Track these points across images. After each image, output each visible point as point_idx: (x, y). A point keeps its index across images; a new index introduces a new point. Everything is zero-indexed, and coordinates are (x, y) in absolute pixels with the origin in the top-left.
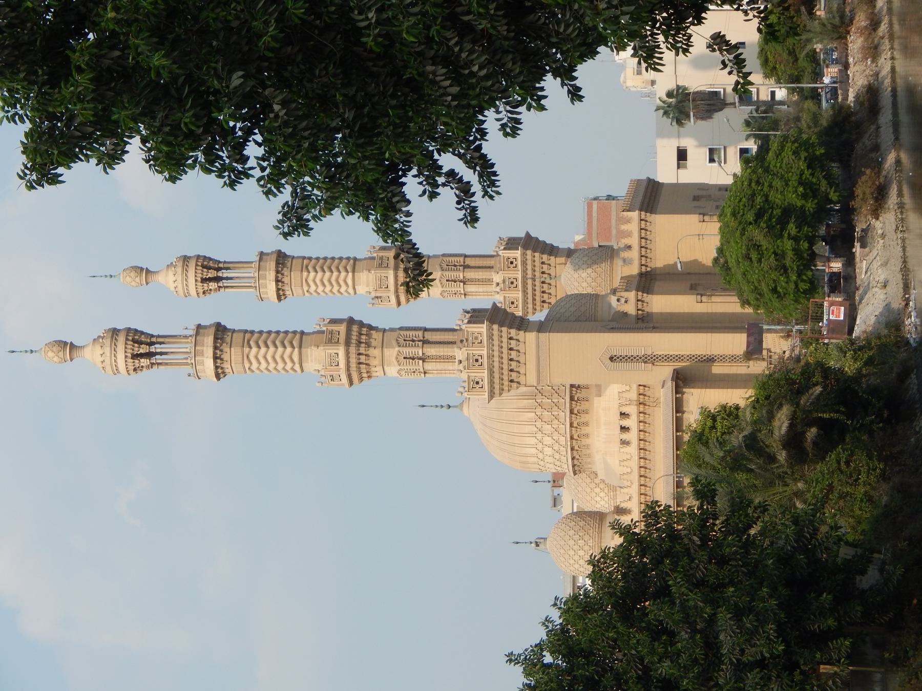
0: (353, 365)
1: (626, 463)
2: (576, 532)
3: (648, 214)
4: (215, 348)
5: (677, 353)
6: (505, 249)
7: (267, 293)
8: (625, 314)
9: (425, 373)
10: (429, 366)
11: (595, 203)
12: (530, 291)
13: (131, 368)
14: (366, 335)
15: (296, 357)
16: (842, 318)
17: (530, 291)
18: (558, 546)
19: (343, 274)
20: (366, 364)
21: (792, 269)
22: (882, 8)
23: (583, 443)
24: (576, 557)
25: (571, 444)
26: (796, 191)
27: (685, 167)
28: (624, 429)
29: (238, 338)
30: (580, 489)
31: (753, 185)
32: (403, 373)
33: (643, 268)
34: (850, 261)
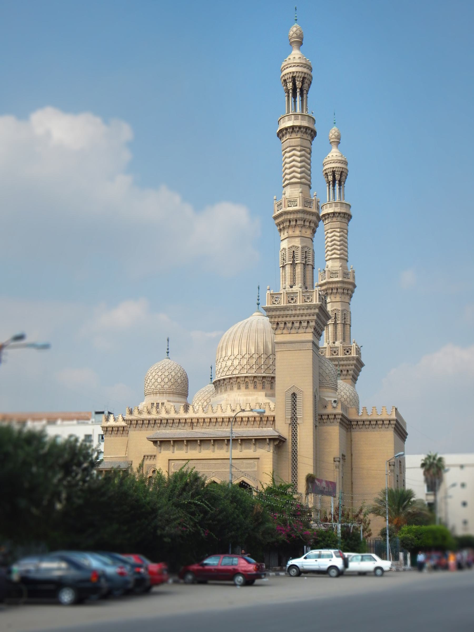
0: (289, 217)
1: (219, 409)
2: (173, 377)
3: (394, 426)
5: (298, 441)
7: (326, 208)
9: (283, 267)
18: (164, 365)
20: (289, 226)
23: (234, 386)
24: (156, 377)
25: (233, 378)
29: (306, 143)
30: (206, 393)
32: (283, 252)
33: (355, 423)
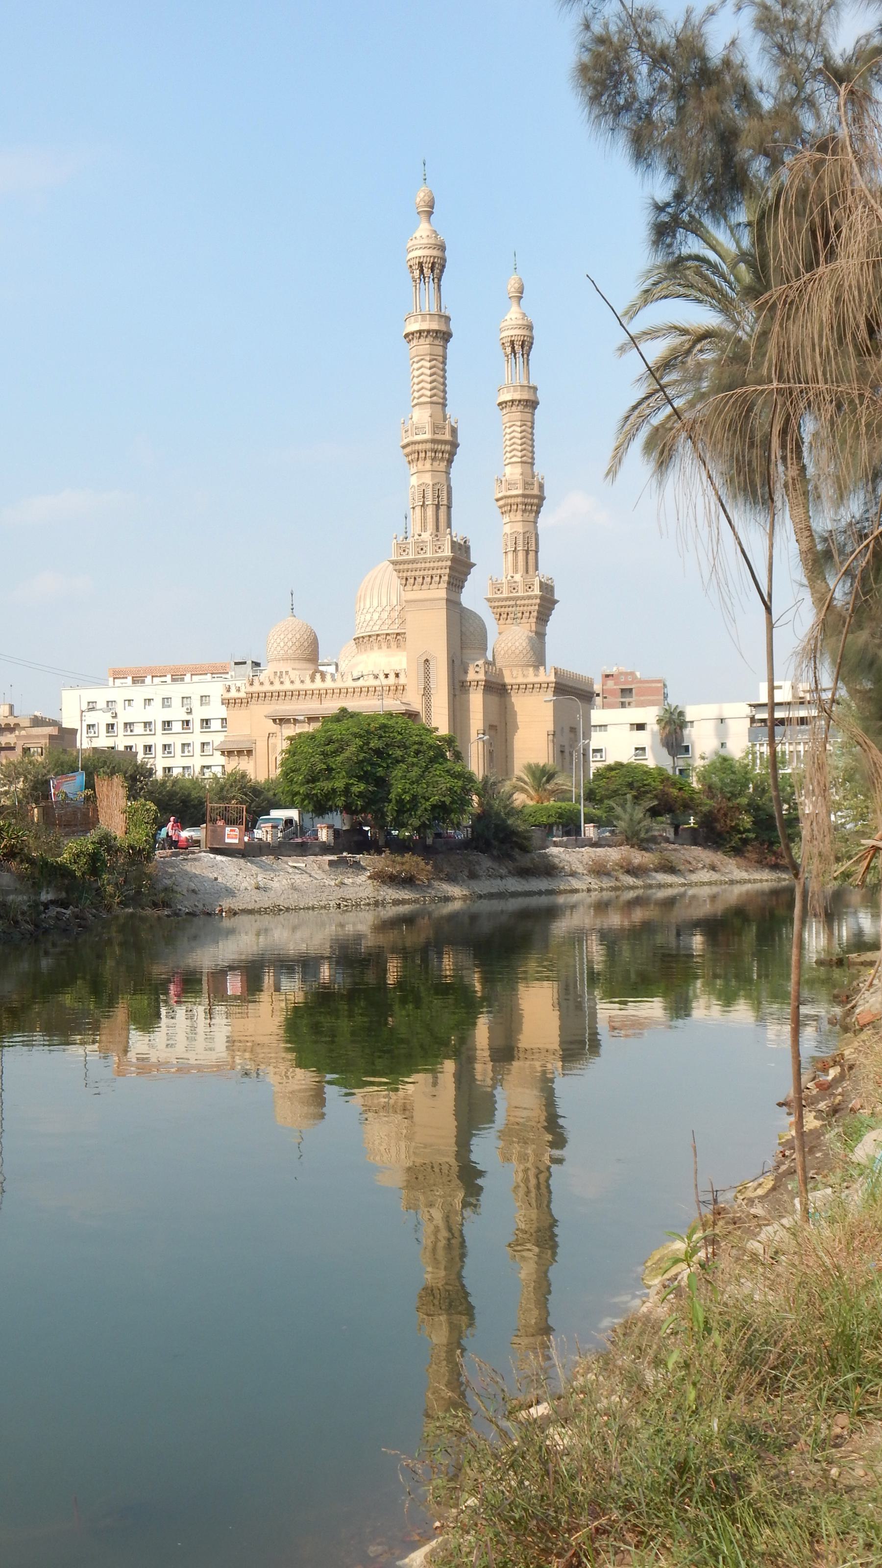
0: (509, 501)
4: (428, 331)
6: (540, 582)
8: (466, 673)
9: (413, 508)
10: (510, 555)
11: (661, 685)
12: (508, 603)
13: (411, 263)
14: (442, 457)
15: (423, 399)
16: (227, 841)
17: (508, 603)
19: (519, 454)
21: (313, 788)
22: (655, 878)
24: (278, 641)
26: (405, 793)
27: (632, 729)
28: (387, 676)
31: (416, 747)
34: (325, 849)
